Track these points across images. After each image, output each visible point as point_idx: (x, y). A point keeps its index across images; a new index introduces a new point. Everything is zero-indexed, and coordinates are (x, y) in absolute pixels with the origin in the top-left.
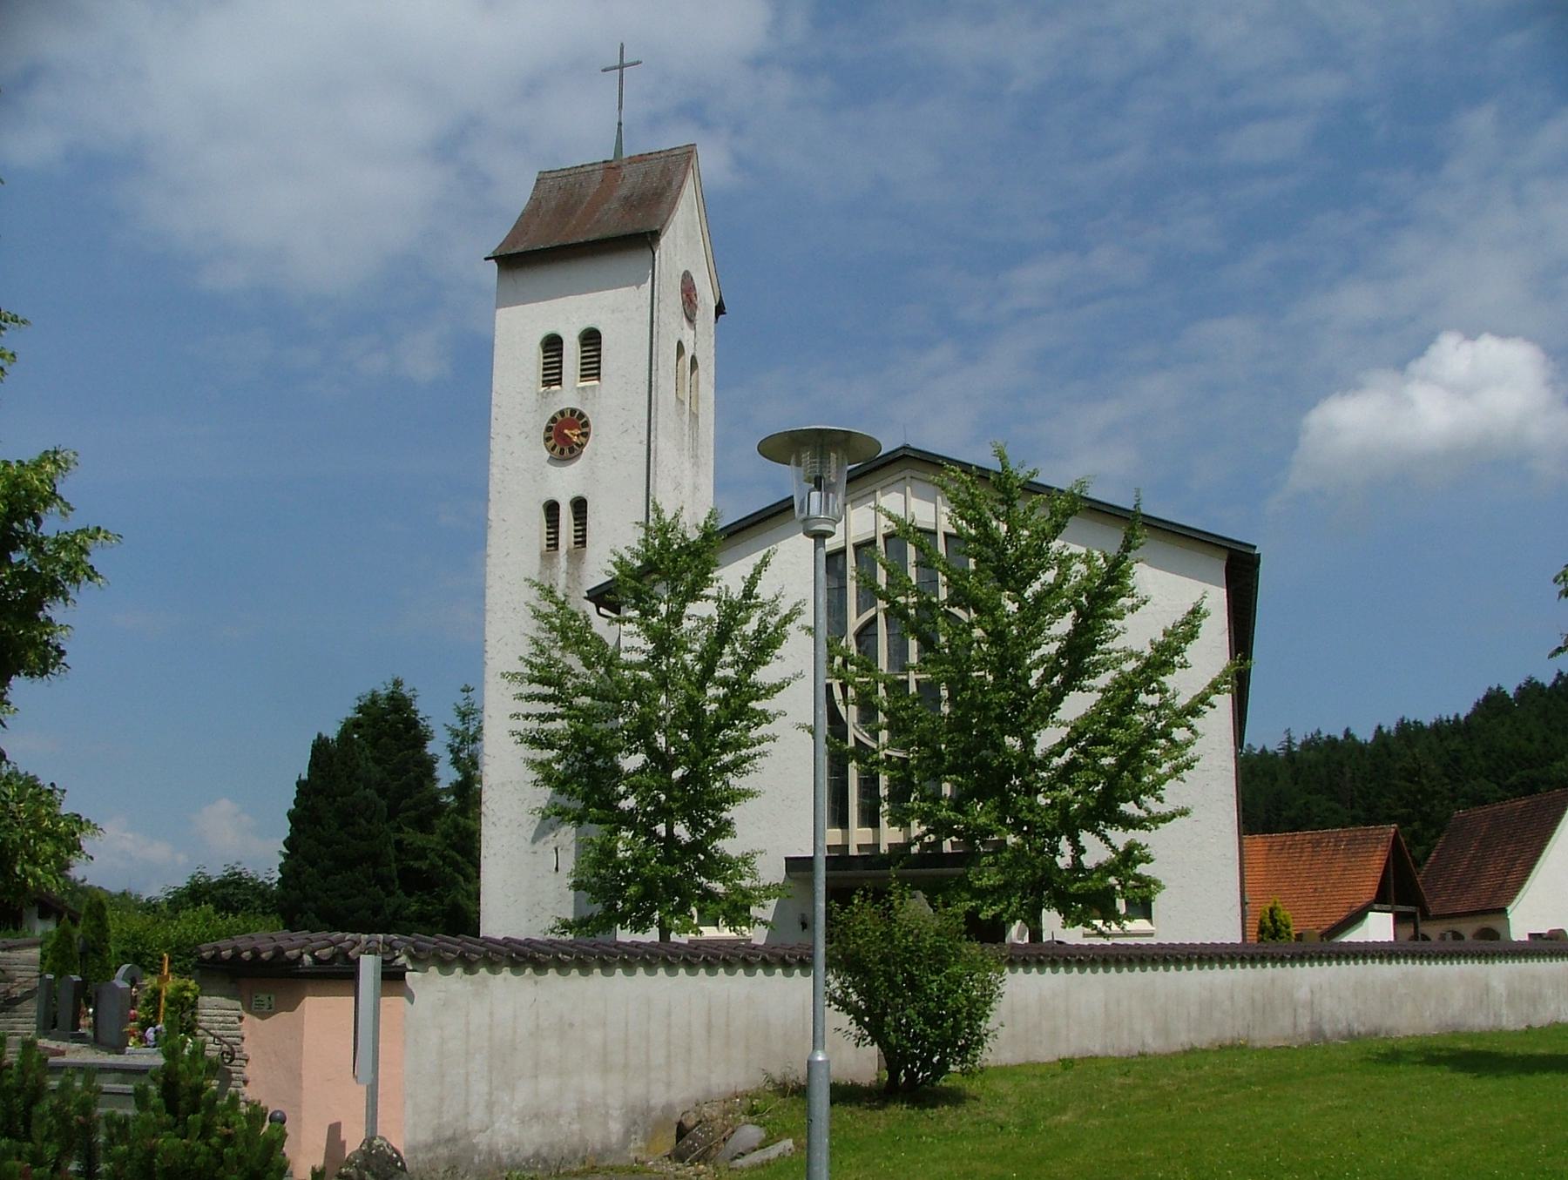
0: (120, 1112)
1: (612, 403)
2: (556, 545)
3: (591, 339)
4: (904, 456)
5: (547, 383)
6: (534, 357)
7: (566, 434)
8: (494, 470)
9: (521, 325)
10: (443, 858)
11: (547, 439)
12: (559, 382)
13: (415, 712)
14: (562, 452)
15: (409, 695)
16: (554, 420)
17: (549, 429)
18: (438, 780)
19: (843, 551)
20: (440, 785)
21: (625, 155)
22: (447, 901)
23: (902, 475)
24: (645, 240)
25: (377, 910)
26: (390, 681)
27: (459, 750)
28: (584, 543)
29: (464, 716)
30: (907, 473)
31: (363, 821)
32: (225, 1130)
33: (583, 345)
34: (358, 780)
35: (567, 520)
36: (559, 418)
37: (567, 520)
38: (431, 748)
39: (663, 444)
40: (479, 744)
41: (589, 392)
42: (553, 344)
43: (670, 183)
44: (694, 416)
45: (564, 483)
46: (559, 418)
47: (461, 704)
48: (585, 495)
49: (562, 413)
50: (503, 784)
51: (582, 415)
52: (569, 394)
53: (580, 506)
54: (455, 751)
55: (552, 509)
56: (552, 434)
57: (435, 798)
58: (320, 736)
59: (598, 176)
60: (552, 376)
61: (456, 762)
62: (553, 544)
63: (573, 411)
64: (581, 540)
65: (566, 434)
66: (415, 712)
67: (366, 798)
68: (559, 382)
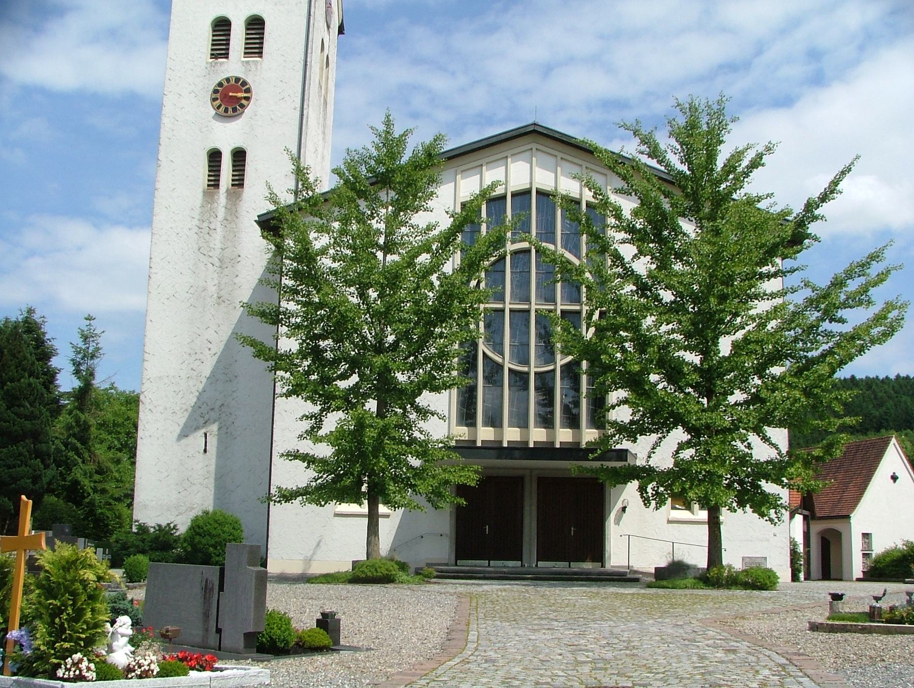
0: (593, 601)
2: (217, 186)
4: (534, 131)
5: (214, 56)
7: (231, 99)
8: (165, 120)
10: (66, 445)
12: (226, 55)
13: (44, 334)
14: (226, 110)
15: (39, 321)
16: (220, 84)
17: (215, 91)
20: (62, 390)
23: (529, 147)
26: (25, 309)
27: (80, 364)
29: (85, 338)
30: (534, 146)
32: (883, 664)
34: (24, 370)
35: (226, 168)
36: (225, 84)
38: (54, 362)
39: (312, 113)
40: (96, 361)
45: (227, 136)
46: (225, 84)
48: (244, 146)
49: (228, 80)
51: (244, 83)
52: (235, 65)
53: (239, 156)
54: (77, 364)
55: (215, 157)
56: (218, 96)
57: (56, 401)
60: (220, 49)
61: (77, 372)
62: (214, 182)
63: (237, 80)
64: (239, 182)
65: (231, 99)
66: (44, 334)
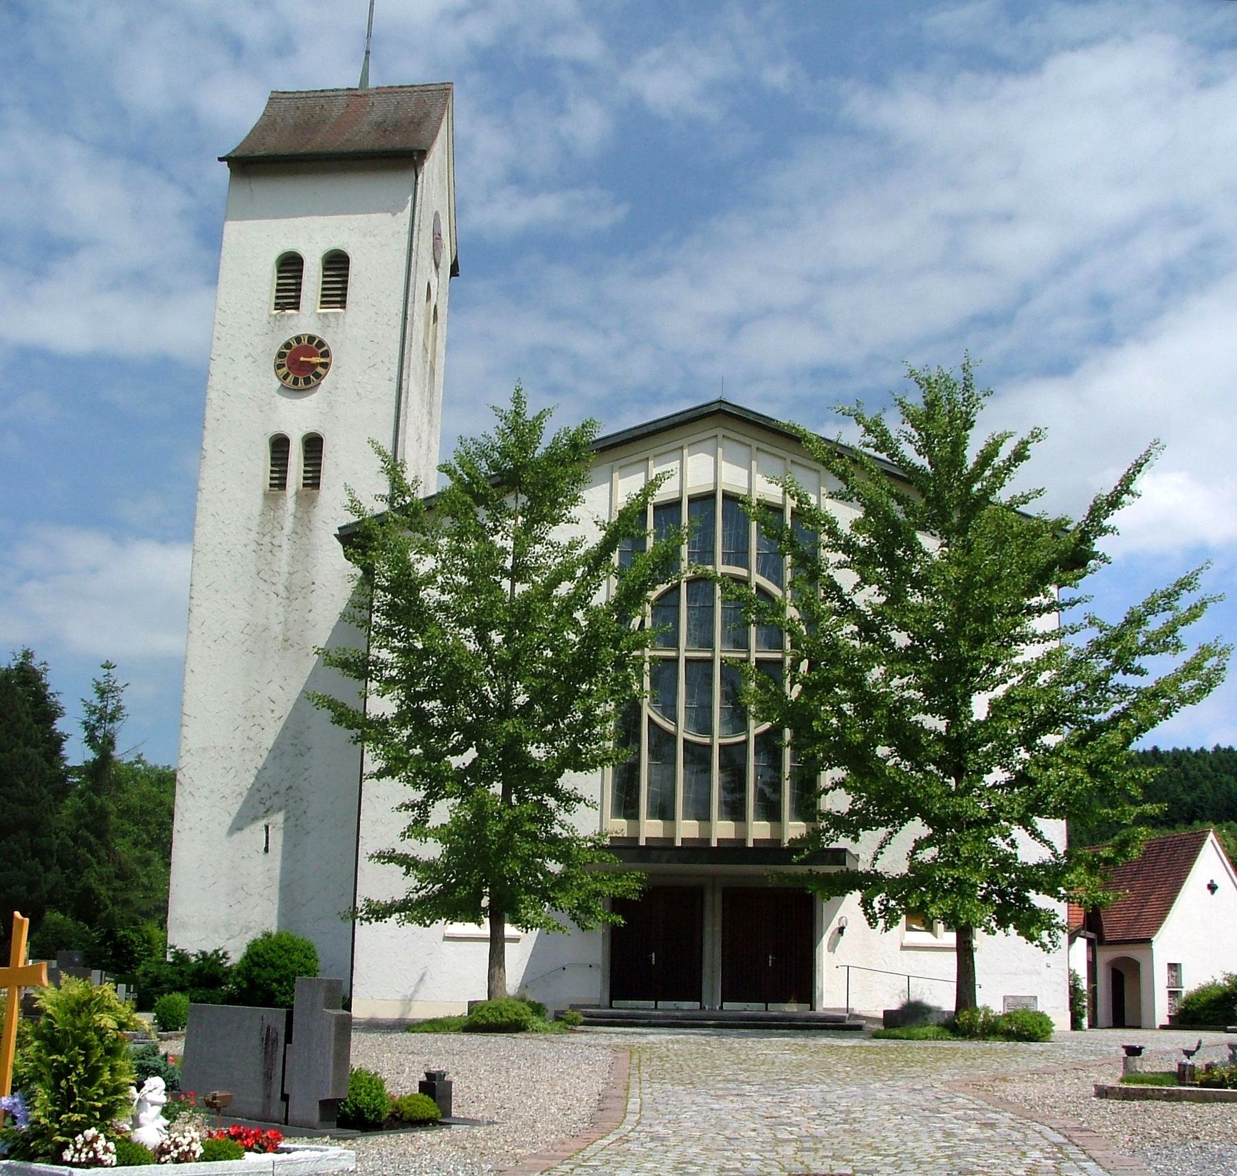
1: (358, 337)
3: (337, 263)
4: (720, 411)
5: (280, 306)
6: (267, 277)
7: (302, 365)
8: (212, 395)
9: (256, 240)
11: (279, 367)
12: (296, 306)
14: (296, 382)
15: (39, 668)
16: (288, 345)
17: (281, 355)
18: (64, 759)
19: (676, 504)
21: (372, 84)
22: (79, 885)
24: (402, 159)
25: (32, 886)
26: (19, 652)
27: (94, 728)
28: (316, 485)
29: (102, 693)
30: (720, 432)
31: (22, 783)
33: (325, 269)
34: (18, 736)
35: (296, 462)
36: (295, 345)
37: (296, 462)
38: (60, 725)
39: (414, 387)
40: (117, 724)
41: (332, 319)
42: (291, 265)
43: (427, 115)
44: (433, 370)
45: (297, 416)
46: (295, 345)
47: (102, 680)
49: (298, 339)
50: (204, 749)
51: (321, 344)
52: (308, 318)
53: (314, 444)
55: (280, 445)
56: (285, 361)
58: (27, 655)
59: (342, 102)
60: (288, 297)
61: (91, 740)
63: (311, 339)
64: (313, 481)
65: (302, 365)
67: (25, 756)
68: (296, 306)
